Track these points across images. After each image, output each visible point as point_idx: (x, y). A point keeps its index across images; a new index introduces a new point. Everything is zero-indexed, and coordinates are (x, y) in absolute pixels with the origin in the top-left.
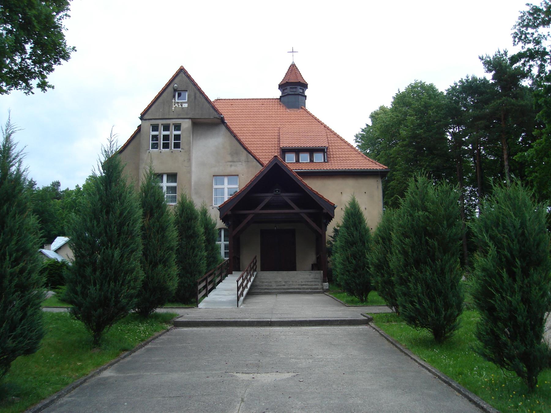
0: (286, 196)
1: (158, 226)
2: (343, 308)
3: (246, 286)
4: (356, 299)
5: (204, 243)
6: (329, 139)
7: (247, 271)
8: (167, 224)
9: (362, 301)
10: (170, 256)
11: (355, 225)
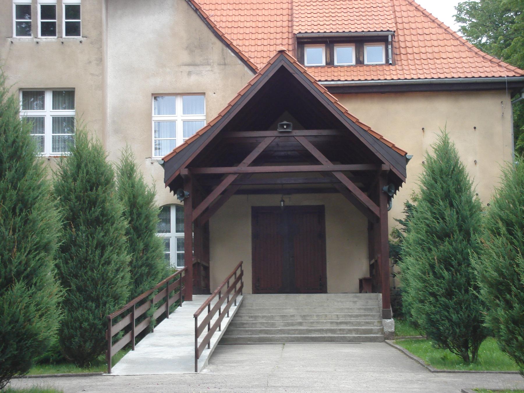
0: (304, 138)
1: (14, 198)
2: (423, 375)
3: (218, 324)
4: (453, 356)
5: (127, 234)
6: (398, 14)
7: (220, 293)
8: (36, 193)
9: (466, 360)
10: (42, 264)
11: (447, 196)
